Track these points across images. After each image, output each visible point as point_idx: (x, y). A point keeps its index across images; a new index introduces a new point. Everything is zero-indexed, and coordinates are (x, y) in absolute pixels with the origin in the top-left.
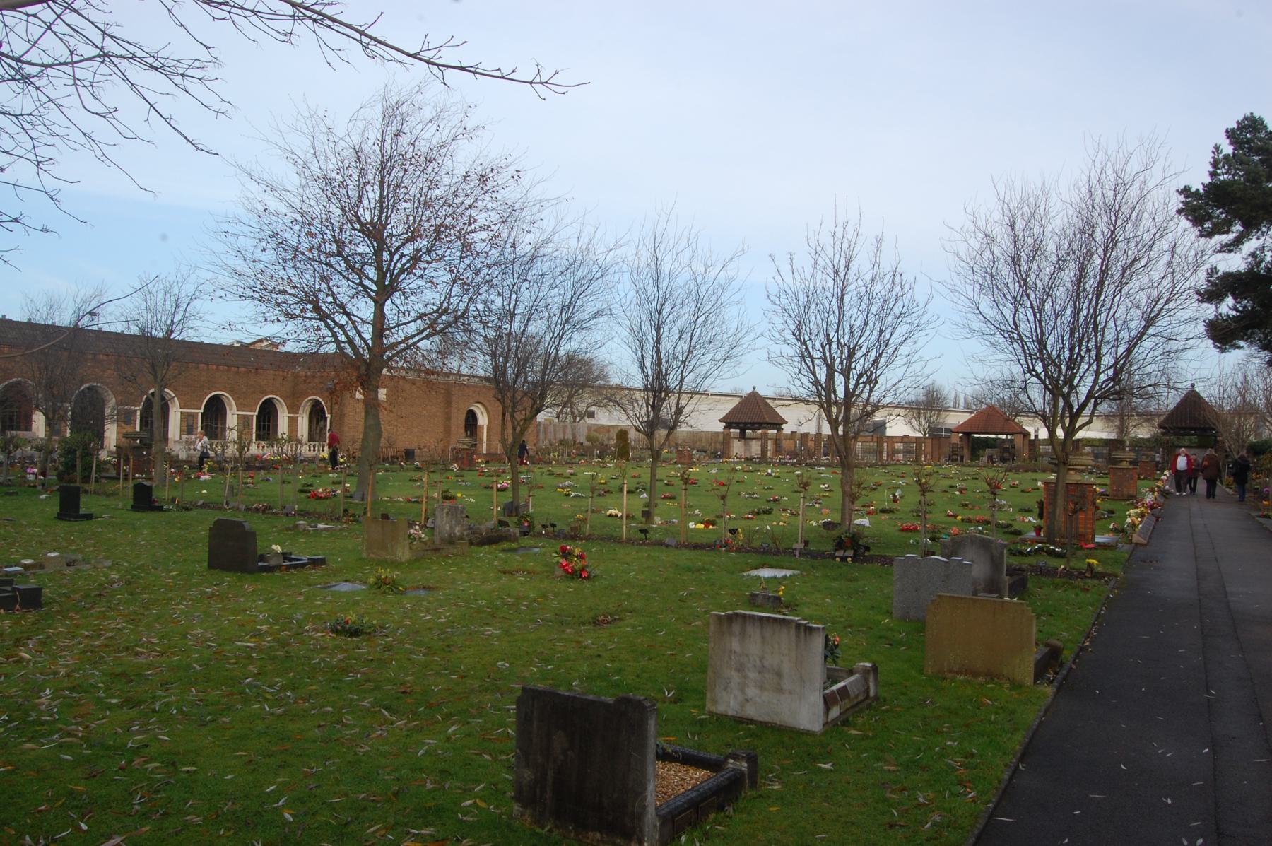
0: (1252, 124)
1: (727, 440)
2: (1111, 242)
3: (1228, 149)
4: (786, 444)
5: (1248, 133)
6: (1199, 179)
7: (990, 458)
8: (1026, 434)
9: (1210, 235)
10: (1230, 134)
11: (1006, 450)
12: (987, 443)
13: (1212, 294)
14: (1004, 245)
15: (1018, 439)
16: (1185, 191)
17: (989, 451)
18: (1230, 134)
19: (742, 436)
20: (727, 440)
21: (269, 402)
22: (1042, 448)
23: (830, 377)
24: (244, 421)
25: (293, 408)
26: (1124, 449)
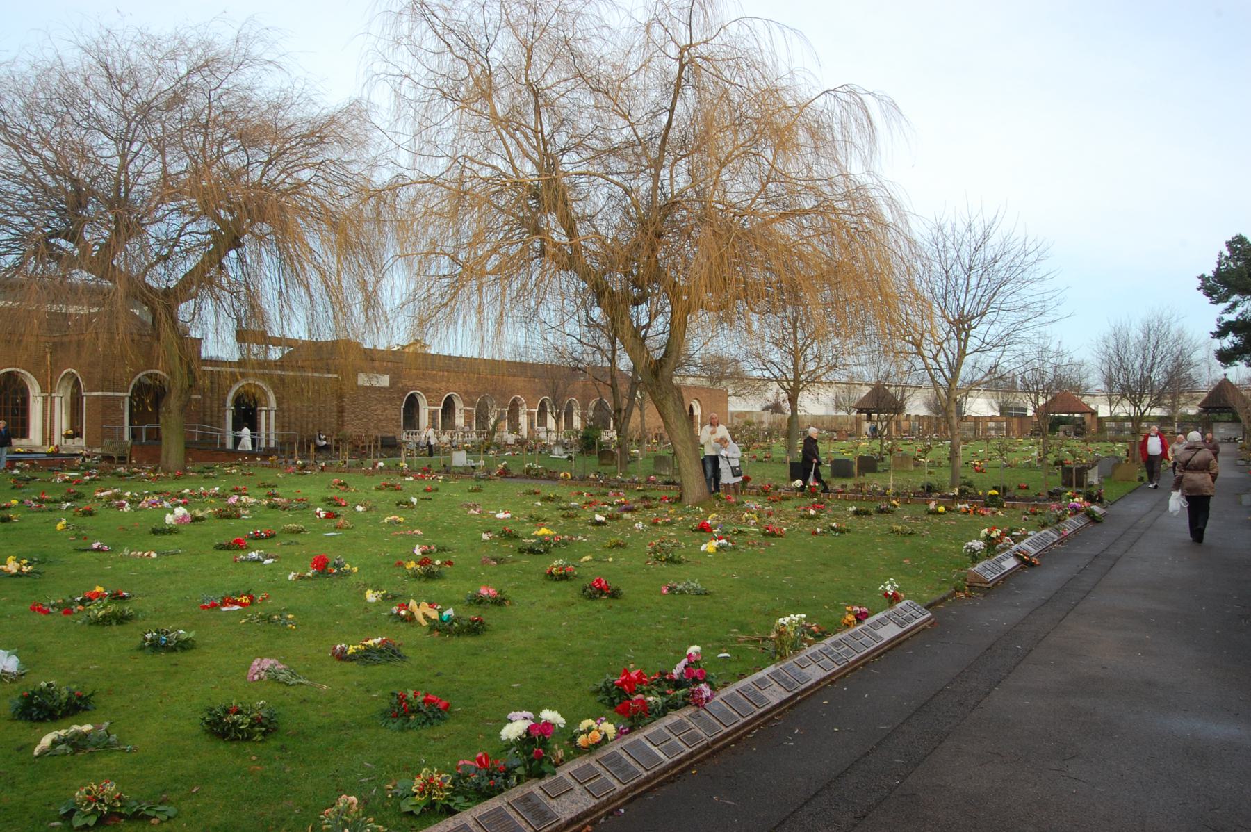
0: (1240, 240)
1: (858, 422)
2: (1156, 346)
3: (1228, 254)
4: (904, 425)
5: (1238, 245)
6: (1209, 270)
7: (1065, 432)
8: (1094, 413)
9: (1217, 303)
10: (1229, 244)
11: (1079, 426)
12: (1060, 421)
13: (1221, 333)
14: (1112, 343)
15: (1088, 417)
16: (1202, 277)
17: (1062, 427)
18: (1229, 244)
19: (869, 419)
20: (858, 422)
21: (449, 397)
22: (1108, 424)
23: (40, 156)
24: (433, 414)
25: (47, 388)
26: (1172, 425)
